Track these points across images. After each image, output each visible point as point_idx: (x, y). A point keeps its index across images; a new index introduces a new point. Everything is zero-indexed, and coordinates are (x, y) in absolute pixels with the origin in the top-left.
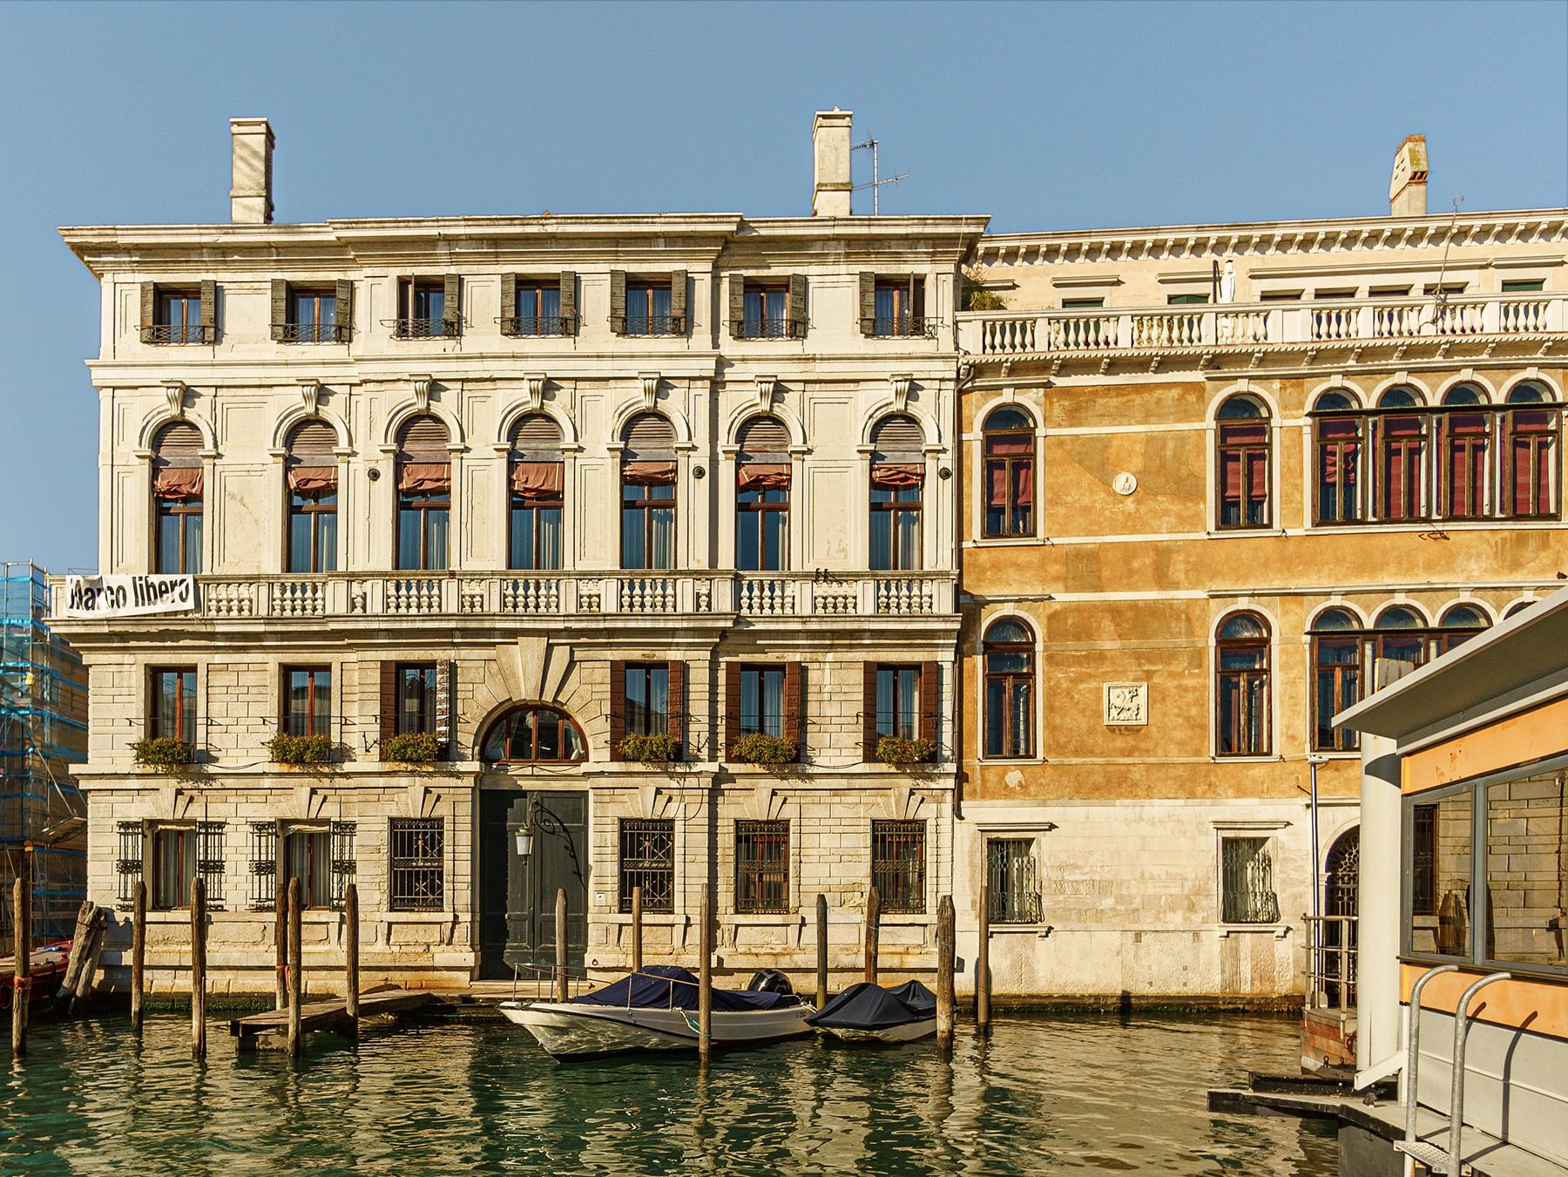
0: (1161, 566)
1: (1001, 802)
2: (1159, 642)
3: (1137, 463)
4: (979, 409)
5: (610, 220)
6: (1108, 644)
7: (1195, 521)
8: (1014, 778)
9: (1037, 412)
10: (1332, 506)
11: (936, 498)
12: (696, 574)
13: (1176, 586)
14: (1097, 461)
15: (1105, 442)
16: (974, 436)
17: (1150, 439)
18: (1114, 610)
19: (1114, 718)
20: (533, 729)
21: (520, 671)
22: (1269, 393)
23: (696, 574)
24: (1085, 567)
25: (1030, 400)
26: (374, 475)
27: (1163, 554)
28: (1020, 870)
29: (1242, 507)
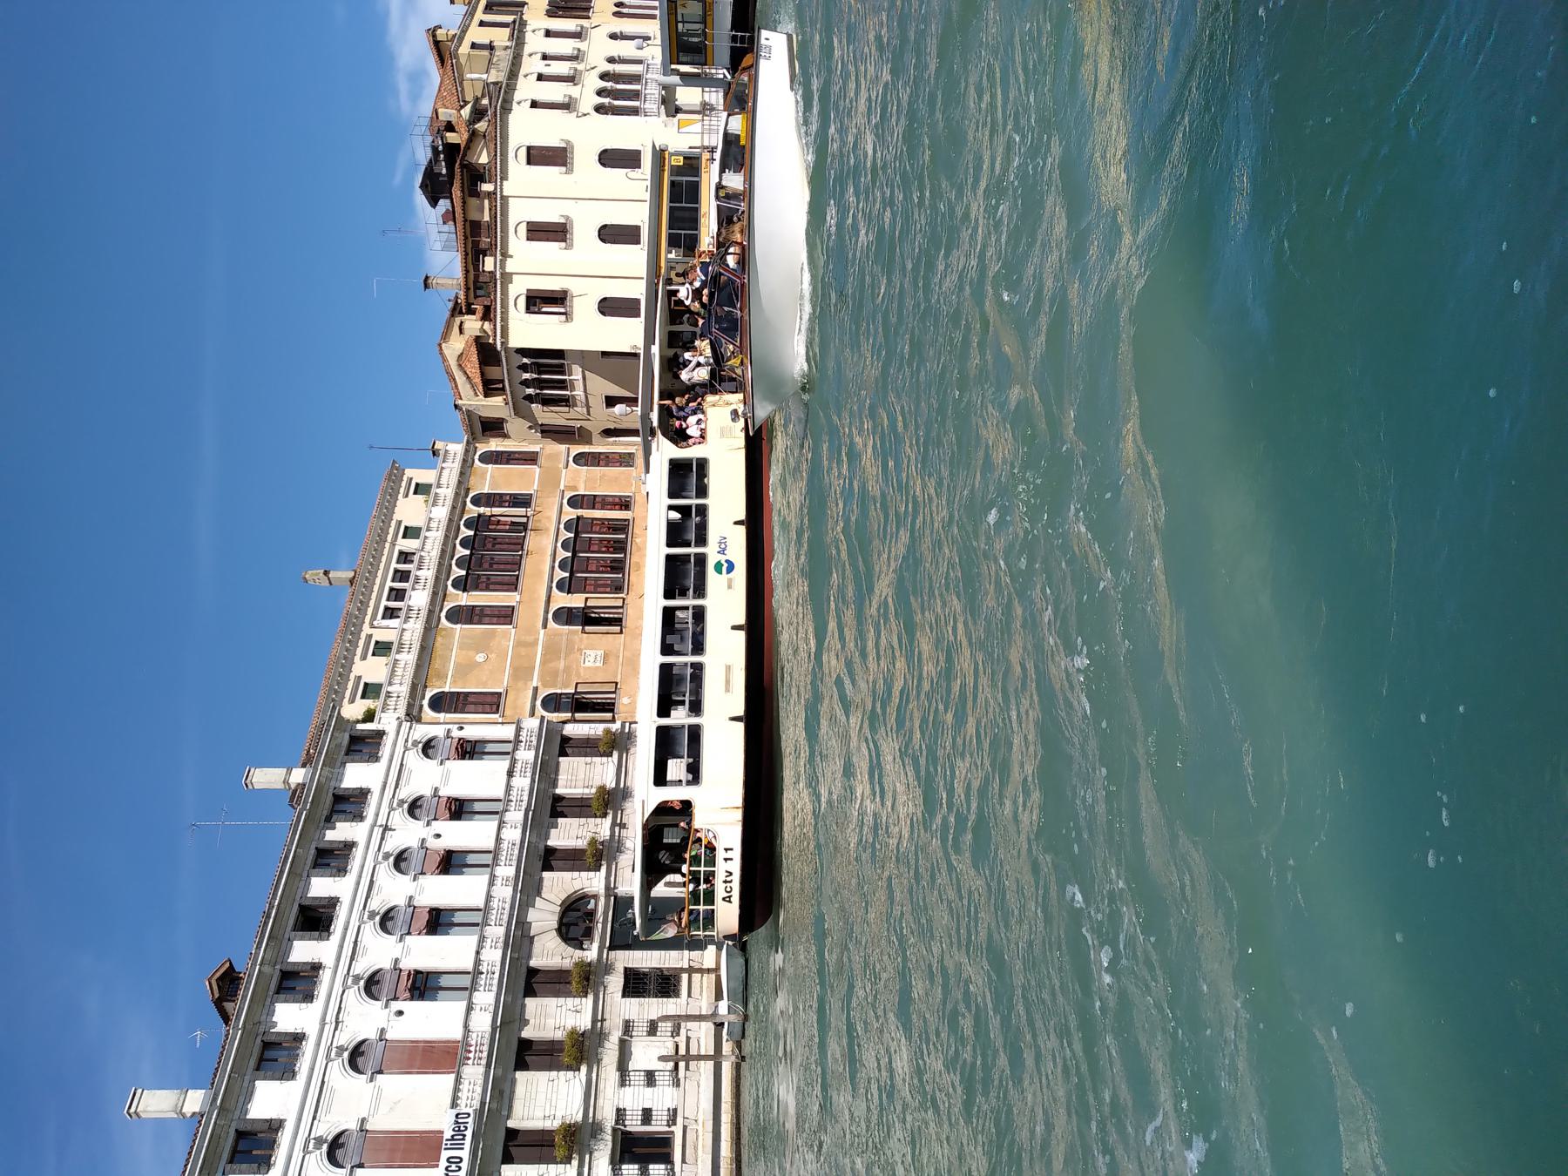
0: (525, 645)
1: (244, 1166)
2: (564, 647)
3: (471, 653)
4: (428, 713)
5: (282, 872)
6: (562, 665)
7: (506, 633)
8: (625, 700)
9: (436, 691)
10: (513, 585)
11: (472, 732)
12: (701, 971)
13: (688, 545)
14: (465, 669)
15: (457, 665)
16: (442, 716)
17: (461, 648)
18: (543, 663)
19: (599, 664)
20: (575, 920)
21: (544, 916)
22: (448, 606)
23: (701, 971)
24: (521, 672)
25: (429, 694)
26: (400, 1013)
27: (518, 644)
28: (1153, 611)
29: (505, 615)
